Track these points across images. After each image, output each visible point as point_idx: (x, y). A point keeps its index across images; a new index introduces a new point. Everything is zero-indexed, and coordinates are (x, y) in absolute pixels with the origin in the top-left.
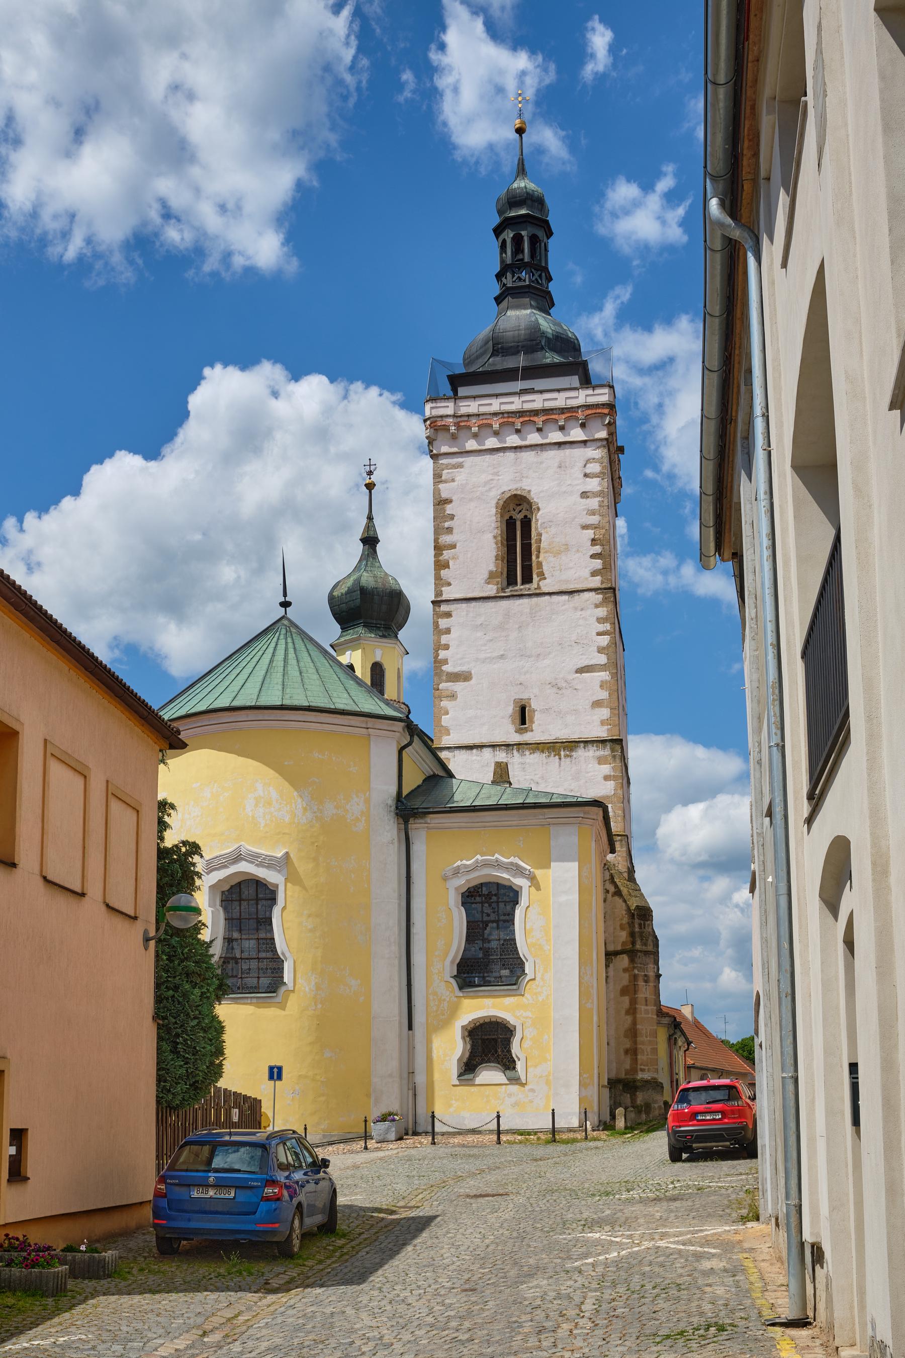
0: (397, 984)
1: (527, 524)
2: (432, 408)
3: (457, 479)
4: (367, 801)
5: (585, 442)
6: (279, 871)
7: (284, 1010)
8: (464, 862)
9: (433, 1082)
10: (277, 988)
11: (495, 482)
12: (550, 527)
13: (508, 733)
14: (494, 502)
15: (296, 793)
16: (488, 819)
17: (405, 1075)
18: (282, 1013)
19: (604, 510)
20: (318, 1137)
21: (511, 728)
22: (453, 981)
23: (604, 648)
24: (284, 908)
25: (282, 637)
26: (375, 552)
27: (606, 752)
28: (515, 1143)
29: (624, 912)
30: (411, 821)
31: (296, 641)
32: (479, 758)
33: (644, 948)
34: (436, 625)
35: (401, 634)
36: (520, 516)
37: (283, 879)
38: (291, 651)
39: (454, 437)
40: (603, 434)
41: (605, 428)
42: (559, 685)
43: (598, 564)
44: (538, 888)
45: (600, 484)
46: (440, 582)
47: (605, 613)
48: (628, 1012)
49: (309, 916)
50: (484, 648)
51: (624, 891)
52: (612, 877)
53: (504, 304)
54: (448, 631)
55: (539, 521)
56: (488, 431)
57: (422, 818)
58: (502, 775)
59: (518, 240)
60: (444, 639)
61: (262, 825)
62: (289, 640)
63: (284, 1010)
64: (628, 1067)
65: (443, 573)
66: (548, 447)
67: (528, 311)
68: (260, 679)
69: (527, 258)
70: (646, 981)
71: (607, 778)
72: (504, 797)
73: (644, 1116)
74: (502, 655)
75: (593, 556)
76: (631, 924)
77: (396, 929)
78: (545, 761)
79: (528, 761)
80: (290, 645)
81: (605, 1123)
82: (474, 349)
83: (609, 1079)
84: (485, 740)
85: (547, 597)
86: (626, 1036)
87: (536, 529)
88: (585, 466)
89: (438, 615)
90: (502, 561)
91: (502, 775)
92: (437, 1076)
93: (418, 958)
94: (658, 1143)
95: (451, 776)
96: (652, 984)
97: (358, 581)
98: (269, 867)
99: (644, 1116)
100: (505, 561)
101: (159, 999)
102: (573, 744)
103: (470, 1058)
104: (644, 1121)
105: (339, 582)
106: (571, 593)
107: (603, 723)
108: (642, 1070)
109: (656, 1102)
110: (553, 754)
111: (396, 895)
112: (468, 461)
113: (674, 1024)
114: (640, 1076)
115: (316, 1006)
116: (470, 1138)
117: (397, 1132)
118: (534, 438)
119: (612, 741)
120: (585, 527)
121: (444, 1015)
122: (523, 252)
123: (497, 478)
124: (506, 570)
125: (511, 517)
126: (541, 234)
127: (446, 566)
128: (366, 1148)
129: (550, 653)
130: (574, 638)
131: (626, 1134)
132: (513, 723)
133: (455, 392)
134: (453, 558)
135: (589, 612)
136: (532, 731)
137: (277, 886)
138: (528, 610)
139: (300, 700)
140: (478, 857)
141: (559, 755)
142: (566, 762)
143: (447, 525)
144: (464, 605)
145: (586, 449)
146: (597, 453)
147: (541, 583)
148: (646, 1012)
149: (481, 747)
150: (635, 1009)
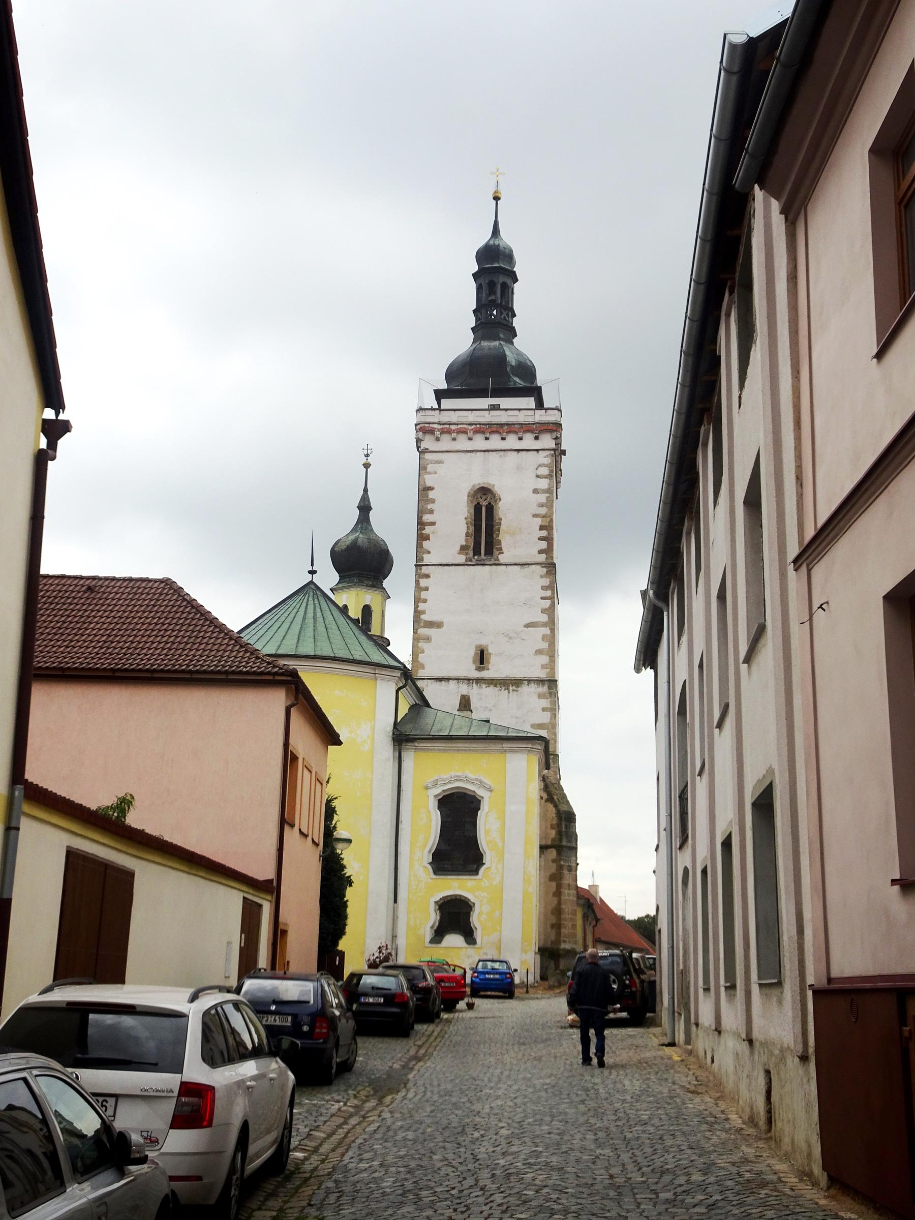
1: (490, 509)
4: (373, 728)
22: (429, 867)
25: (311, 598)
27: (544, 689)
33: (569, 844)
34: (417, 583)
35: (386, 584)
36: (484, 503)
38: (318, 610)
43: (544, 545)
54: (426, 589)
58: (465, 704)
60: (423, 595)
62: (316, 601)
67: (497, 343)
68: (297, 632)
71: (544, 710)
72: (473, 729)
76: (559, 825)
80: (317, 605)
91: (465, 704)
93: (403, 848)
95: (428, 705)
97: (356, 540)
105: (339, 540)
108: (564, 942)
114: (563, 946)
120: (535, 516)
122: (495, 293)
125: (478, 503)
127: (427, 538)
132: (474, 662)
133: (439, 403)
139: (327, 652)
146: (544, 458)
148: (568, 895)
149: (448, 679)
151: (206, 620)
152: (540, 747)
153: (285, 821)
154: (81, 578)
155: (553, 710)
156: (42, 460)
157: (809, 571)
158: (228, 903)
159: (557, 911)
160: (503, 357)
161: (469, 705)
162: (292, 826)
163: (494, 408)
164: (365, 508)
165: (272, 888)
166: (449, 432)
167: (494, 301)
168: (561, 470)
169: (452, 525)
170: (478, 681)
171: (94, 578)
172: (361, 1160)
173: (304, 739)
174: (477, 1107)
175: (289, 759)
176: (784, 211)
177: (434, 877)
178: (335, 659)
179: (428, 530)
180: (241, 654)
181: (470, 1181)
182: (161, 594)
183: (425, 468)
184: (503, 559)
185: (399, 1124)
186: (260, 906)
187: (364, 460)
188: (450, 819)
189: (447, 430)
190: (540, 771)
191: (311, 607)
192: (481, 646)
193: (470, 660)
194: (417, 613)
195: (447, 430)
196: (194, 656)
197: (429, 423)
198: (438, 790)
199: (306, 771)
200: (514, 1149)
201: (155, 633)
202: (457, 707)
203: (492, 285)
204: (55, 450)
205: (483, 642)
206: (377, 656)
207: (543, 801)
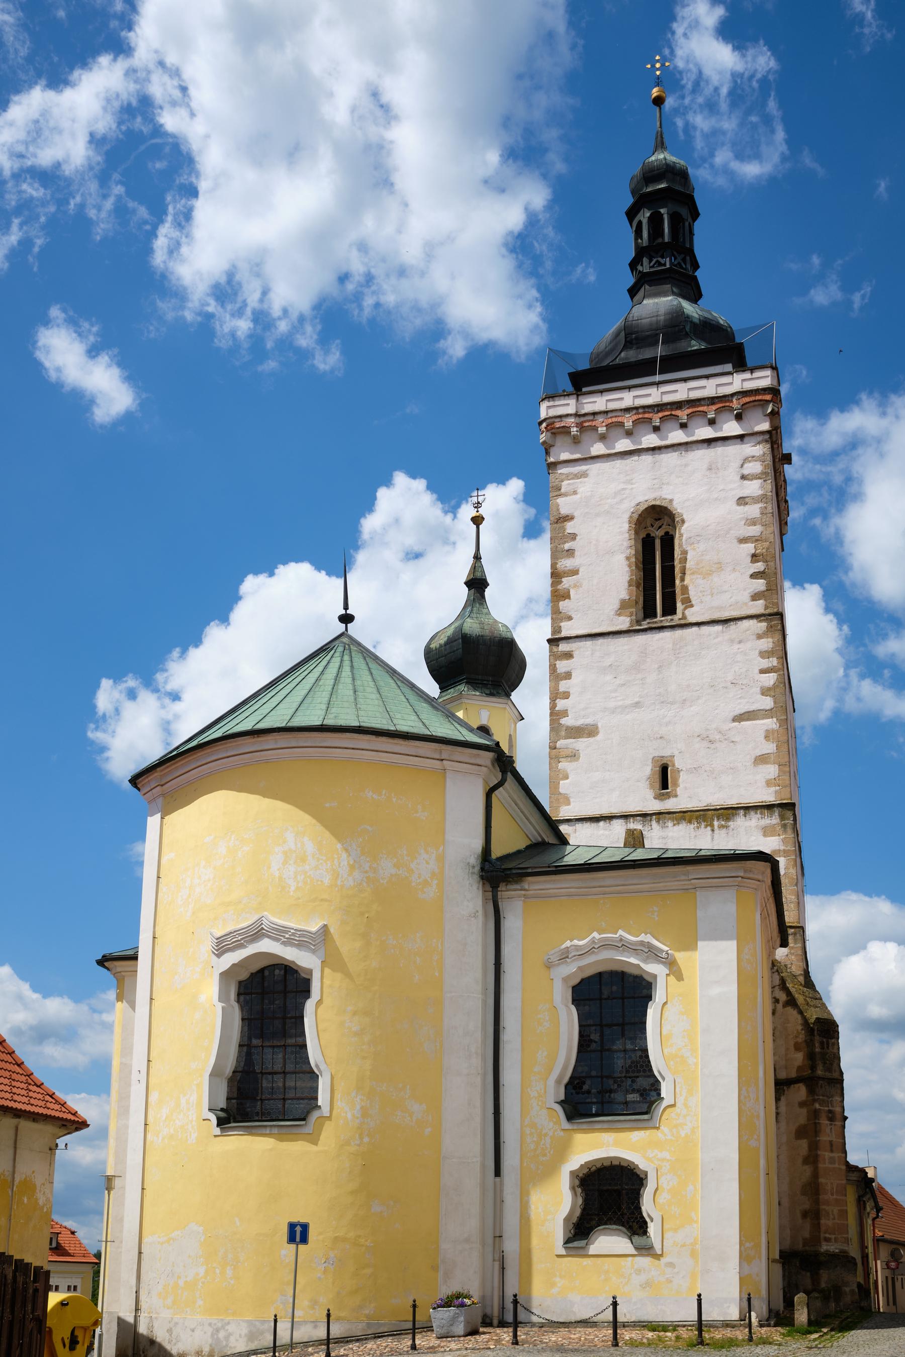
1: (668, 542)
2: (549, 407)
3: (580, 490)
5: (741, 437)
6: (314, 952)
7: (316, 1144)
8: (576, 942)
9: (529, 1251)
10: (308, 1113)
11: (627, 492)
12: (699, 542)
13: (645, 799)
14: (626, 517)
15: (339, 846)
16: (608, 882)
17: (490, 1240)
18: (314, 1148)
19: (768, 519)
20: (360, 1326)
21: (649, 794)
22: (558, 1108)
23: (769, 689)
24: (319, 1003)
25: (337, 654)
26: (483, 597)
27: (774, 819)
28: (642, 1344)
29: (800, 1028)
30: (502, 887)
31: (355, 659)
32: (607, 833)
33: (828, 1075)
34: (553, 669)
35: (514, 696)
36: (660, 533)
37: (319, 962)
39: (576, 441)
40: (765, 426)
41: (768, 418)
42: (711, 737)
43: (760, 585)
44: (680, 978)
45: (762, 487)
46: (558, 617)
47: (771, 645)
48: (806, 1161)
49: (355, 1013)
50: (614, 695)
51: (800, 999)
52: (783, 982)
53: (641, 293)
54: (568, 675)
55: (684, 536)
56: (619, 431)
57: (516, 882)
58: (635, 840)
59: (656, 221)
60: (563, 686)
61: (293, 888)
62: (346, 658)
63: (316, 1144)
65: (563, 605)
66: (694, 446)
67: (670, 298)
68: (299, 699)
74: (637, 703)
75: (754, 576)
76: (809, 1043)
77: (479, 1035)
78: (693, 834)
79: (670, 834)
81: (777, 1314)
82: (602, 347)
83: (781, 1251)
84: (615, 810)
85: (695, 629)
86: (804, 1193)
87: (681, 545)
88: (742, 466)
89: (555, 657)
90: (638, 587)
91: (635, 840)
92: (535, 1242)
96: (839, 1123)
97: (460, 628)
98: (300, 945)
100: (641, 588)
102: (730, 811)
103: (582, 1218)
106: (726, 621)
107: (769, 783)
108: (827, 1240)
110: (703, 825)
112: (594, 468)
113: (863, 1183)
114: (824, 1247)
115: (361, 1138)
116: (578, 1334)
117: (467, 1323)
118: (677, 436)
119: (781, 806)
121: (545, 1155)
123: (630, 486)
124: (641, 599)
125: (648, 535)
126: (684, 212)
127: (566, 596)
128: (414, 1347)
129: (699, 698)
130: (730, 677)
131: (811, 1333)
132: (652, 786)
134: (575, 586)
135: (749, 645)
136: (676, 796)
137: (310, 972)
138: (670, 646)
140: (595, 935)
141: (712, 826)
143: (567, 546)
144: (589, 643)
145: (744, 446)
146: (758, 449)
147: (687, 612)
149: (610, 818)
150: (817, 1156)
159: (813, 1189)
194: (556, 715)
205: (666, 753)
207: (780, 1006)
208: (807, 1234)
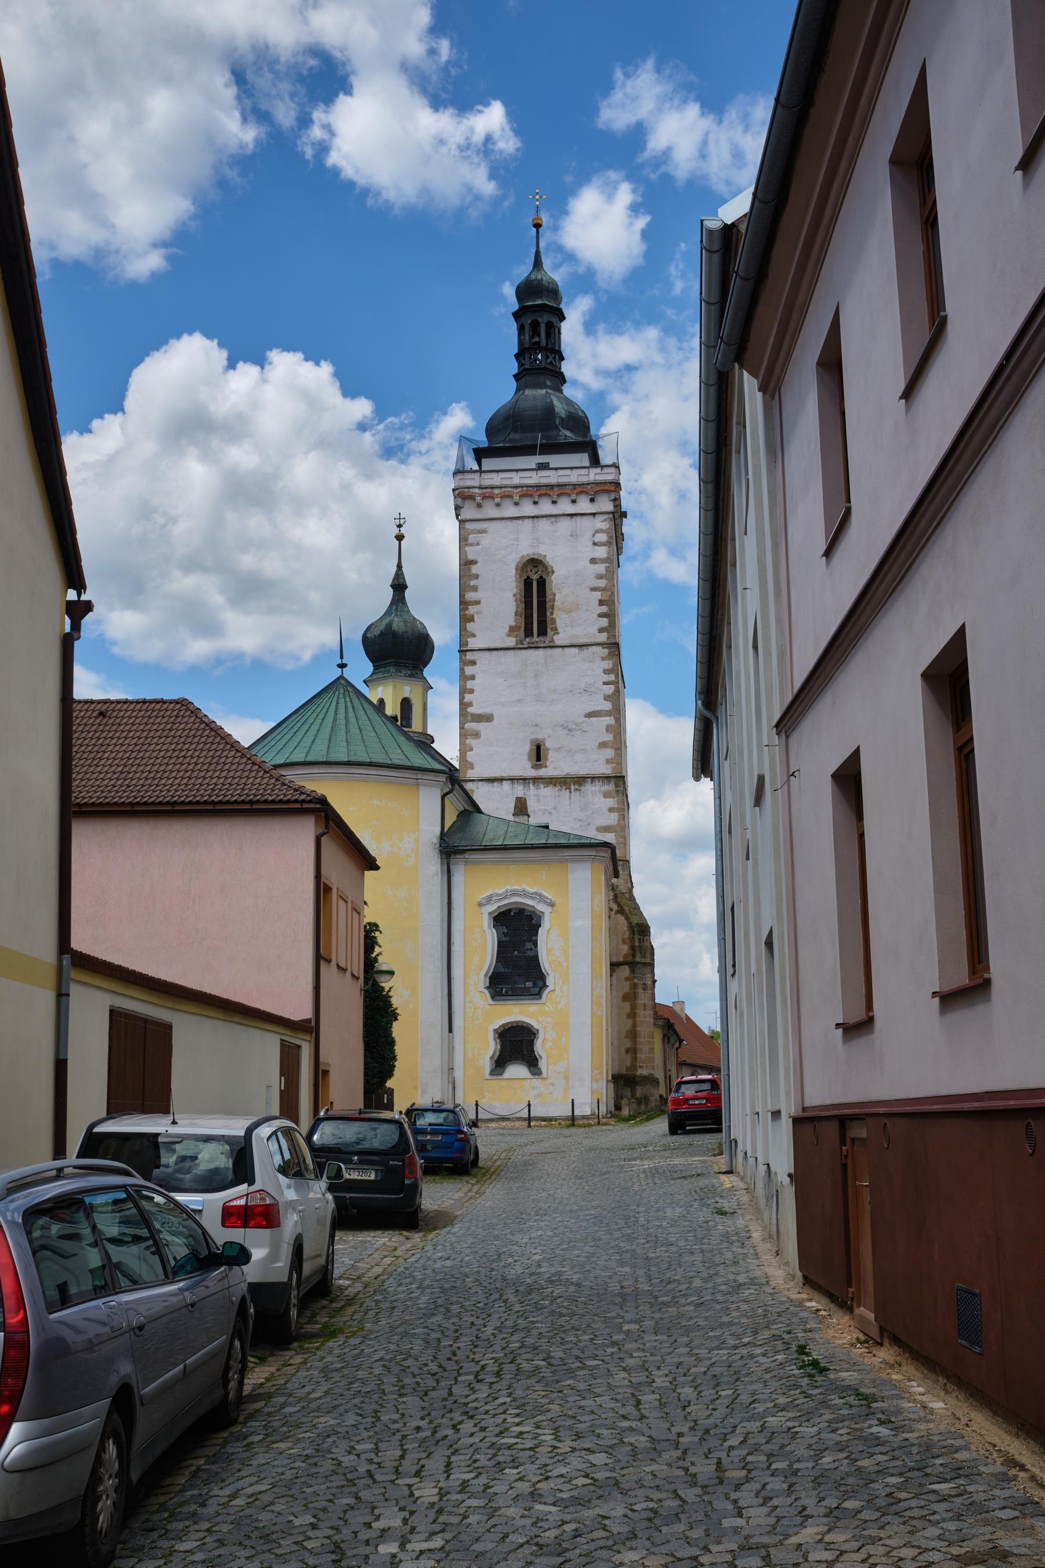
0: (439, 994)
1: (542, 583)
14: (513, 566)
17: (446, 1070)
21: (529, 765)
22: (486, 991)
25: (341, 696)
27: (610, 787)
33: (643, 960)
34: (462, 671)
35: (427, 672)
36: (535, 577)
38: (350, 709)
39: (479, 506)
43: (604, 622)
48: (629, 1016)
53: (523, 380)
54: (473, 678)
55: (555, 582)
58: (521, 808)
59: (535, 325)
60: (470, 684)
62: (348, 699)
64: (629, 1064)
67: (544, 391)
68: (328, 735)
69: (544, 343)
70: (645, 989)
71: (611, 810)
72: (530, 836)
73: (643, 1107)
75: (600, 615)
76: (632, 940)
77: (439, 948)
80: (349, 704)
86: (627, 1037)
91: (521, 808)
93: (457, 972)
94: (661, 1125)
95: (479, 811)
96: (650, 992)
97: (389, 626)
99: (643, 1107)
101: (365, 1025)
104: (644, 1112)
105: (372, 625)
108: (641, 1067)
109: (653, 1095)
111: (439, 919)
116: (504, 1124)
120: (593, 589)
122: (539, 335)
127: (471, 619)
130: (583, 686)
132: (530, 759)
134: (478, 613)
141: (570, 789)
142: (576, 795)
146: (602, 523)
148: (645, 1017)
149: (500, 780)
151: (227, 743)
152: (606, 854)
153: (319, 958)
154: (92, 702)
155: (623, 808)
156: (68, 643)
157: (787, 737)
158: (268, 1047)
160: (550, 409)
161: (526, 808)
162: (329, 961)
163: (543, 467)
164: (399, 586)
165: (310, 1028)
166: (492, 497)
167: (538, 343)
168: (622, 534)
169: (500, 604)
170: (535, 780)
171: (105, 702)
172: (400, 1285)
173: (338, 868)
174: (518, 1237)
175: (322, 891)
176: (763, 388)
177: (492, 1002)
178: (371, 765)
179: (472, 610)
180: (265, 781)
181: (496, 1296)
182: (177, 716)
183: (466, 540)
184: (559, 640)
185: (440, 1254)
186: (299, 1047)
187: (396, 531)
188: (507, 939)
189: (488, 494)
190: (607, 880)
191: (342, 706)
192: (537, 740)
193: (525, 758)
194: (464, 706)
195: (488, 494)
196: (216, 785)
197: (468, 488)
198: (492, 907)
199: (341, 902)
200: (542, 1270)
201: (173, 761)
202: (512, 811)
203: (535, 325)
204: (79, 630)
205: (539, 736)
206: (419, 759)
207: (613, 913)
208: (629, 1064)
